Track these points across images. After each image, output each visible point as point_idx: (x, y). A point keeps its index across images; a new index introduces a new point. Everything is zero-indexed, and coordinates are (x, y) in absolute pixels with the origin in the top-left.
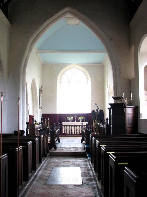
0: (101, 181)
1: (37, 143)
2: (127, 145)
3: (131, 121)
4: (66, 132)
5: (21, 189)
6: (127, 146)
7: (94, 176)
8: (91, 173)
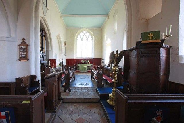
2: (141, 97)
6: (139, 96)
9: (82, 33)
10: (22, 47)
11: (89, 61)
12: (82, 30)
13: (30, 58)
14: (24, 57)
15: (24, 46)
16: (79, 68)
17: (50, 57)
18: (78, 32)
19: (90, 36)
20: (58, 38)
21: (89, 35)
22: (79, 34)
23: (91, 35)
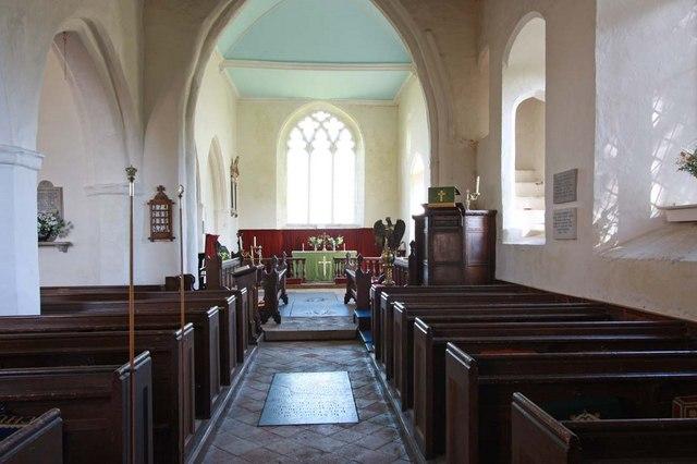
0: (412, 412)
1: (232, 311)
3: (477, 249)
4: (300, 277)
5: (192, 445)
7: (386, 397)
8: (378, 387)
9: (308, 119)
10: (158, 207)
11: (340, 240)
12: (309, 106)
13: (176, 232)
14: (164, 232)
16: (296, 268)
19: (347, 134)
21: (340, 131)
22: (295, 124)
23: (350, 127)
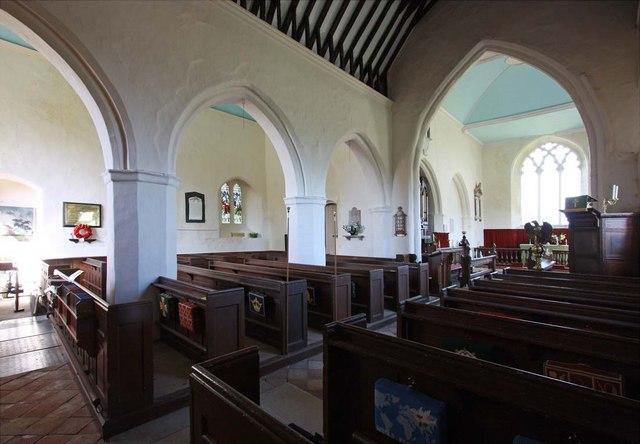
11: (563, 237)
12: (536, 141)
14: (402, 230)
15: (402, 218)
17: (438, 229)
18: (523, 151)
19: (573, 157)
20: (458, 183)
21: (567, 154)
22: (527, 155)
23: (574, 150)
